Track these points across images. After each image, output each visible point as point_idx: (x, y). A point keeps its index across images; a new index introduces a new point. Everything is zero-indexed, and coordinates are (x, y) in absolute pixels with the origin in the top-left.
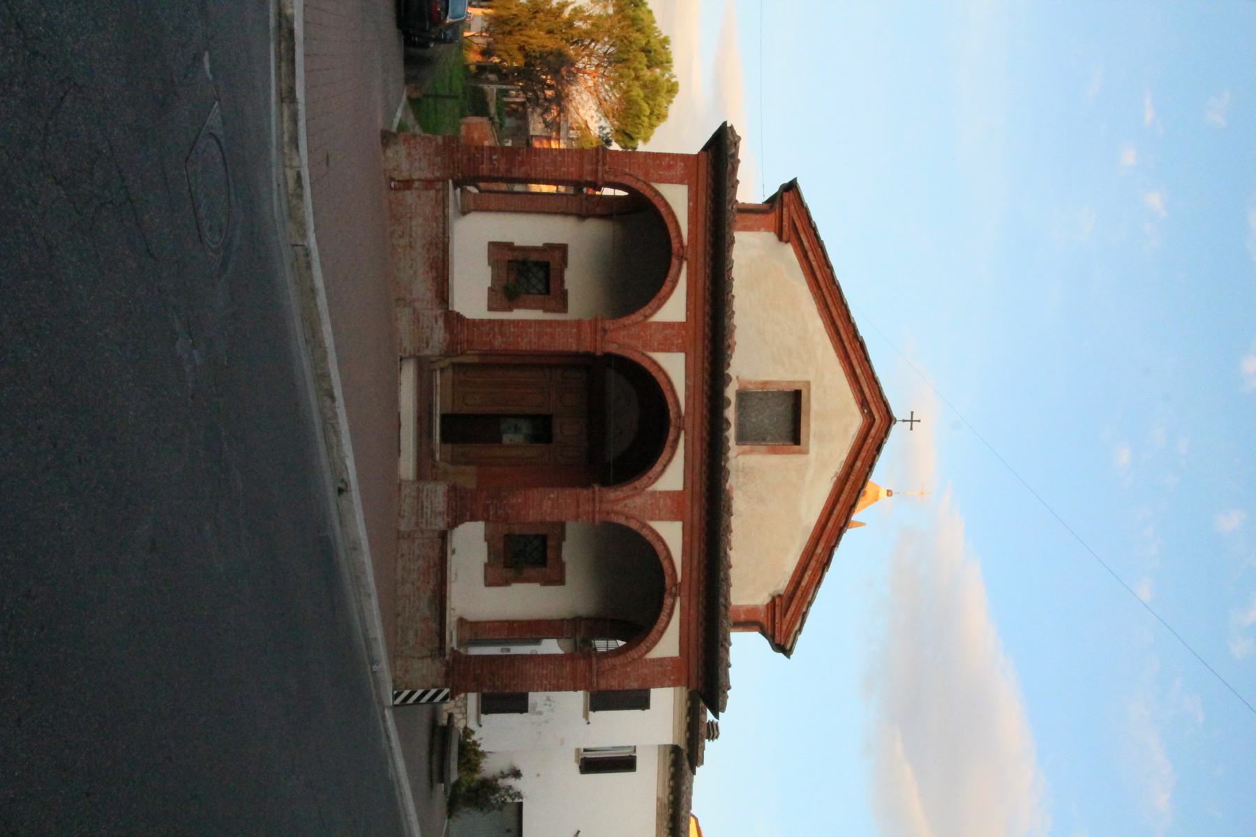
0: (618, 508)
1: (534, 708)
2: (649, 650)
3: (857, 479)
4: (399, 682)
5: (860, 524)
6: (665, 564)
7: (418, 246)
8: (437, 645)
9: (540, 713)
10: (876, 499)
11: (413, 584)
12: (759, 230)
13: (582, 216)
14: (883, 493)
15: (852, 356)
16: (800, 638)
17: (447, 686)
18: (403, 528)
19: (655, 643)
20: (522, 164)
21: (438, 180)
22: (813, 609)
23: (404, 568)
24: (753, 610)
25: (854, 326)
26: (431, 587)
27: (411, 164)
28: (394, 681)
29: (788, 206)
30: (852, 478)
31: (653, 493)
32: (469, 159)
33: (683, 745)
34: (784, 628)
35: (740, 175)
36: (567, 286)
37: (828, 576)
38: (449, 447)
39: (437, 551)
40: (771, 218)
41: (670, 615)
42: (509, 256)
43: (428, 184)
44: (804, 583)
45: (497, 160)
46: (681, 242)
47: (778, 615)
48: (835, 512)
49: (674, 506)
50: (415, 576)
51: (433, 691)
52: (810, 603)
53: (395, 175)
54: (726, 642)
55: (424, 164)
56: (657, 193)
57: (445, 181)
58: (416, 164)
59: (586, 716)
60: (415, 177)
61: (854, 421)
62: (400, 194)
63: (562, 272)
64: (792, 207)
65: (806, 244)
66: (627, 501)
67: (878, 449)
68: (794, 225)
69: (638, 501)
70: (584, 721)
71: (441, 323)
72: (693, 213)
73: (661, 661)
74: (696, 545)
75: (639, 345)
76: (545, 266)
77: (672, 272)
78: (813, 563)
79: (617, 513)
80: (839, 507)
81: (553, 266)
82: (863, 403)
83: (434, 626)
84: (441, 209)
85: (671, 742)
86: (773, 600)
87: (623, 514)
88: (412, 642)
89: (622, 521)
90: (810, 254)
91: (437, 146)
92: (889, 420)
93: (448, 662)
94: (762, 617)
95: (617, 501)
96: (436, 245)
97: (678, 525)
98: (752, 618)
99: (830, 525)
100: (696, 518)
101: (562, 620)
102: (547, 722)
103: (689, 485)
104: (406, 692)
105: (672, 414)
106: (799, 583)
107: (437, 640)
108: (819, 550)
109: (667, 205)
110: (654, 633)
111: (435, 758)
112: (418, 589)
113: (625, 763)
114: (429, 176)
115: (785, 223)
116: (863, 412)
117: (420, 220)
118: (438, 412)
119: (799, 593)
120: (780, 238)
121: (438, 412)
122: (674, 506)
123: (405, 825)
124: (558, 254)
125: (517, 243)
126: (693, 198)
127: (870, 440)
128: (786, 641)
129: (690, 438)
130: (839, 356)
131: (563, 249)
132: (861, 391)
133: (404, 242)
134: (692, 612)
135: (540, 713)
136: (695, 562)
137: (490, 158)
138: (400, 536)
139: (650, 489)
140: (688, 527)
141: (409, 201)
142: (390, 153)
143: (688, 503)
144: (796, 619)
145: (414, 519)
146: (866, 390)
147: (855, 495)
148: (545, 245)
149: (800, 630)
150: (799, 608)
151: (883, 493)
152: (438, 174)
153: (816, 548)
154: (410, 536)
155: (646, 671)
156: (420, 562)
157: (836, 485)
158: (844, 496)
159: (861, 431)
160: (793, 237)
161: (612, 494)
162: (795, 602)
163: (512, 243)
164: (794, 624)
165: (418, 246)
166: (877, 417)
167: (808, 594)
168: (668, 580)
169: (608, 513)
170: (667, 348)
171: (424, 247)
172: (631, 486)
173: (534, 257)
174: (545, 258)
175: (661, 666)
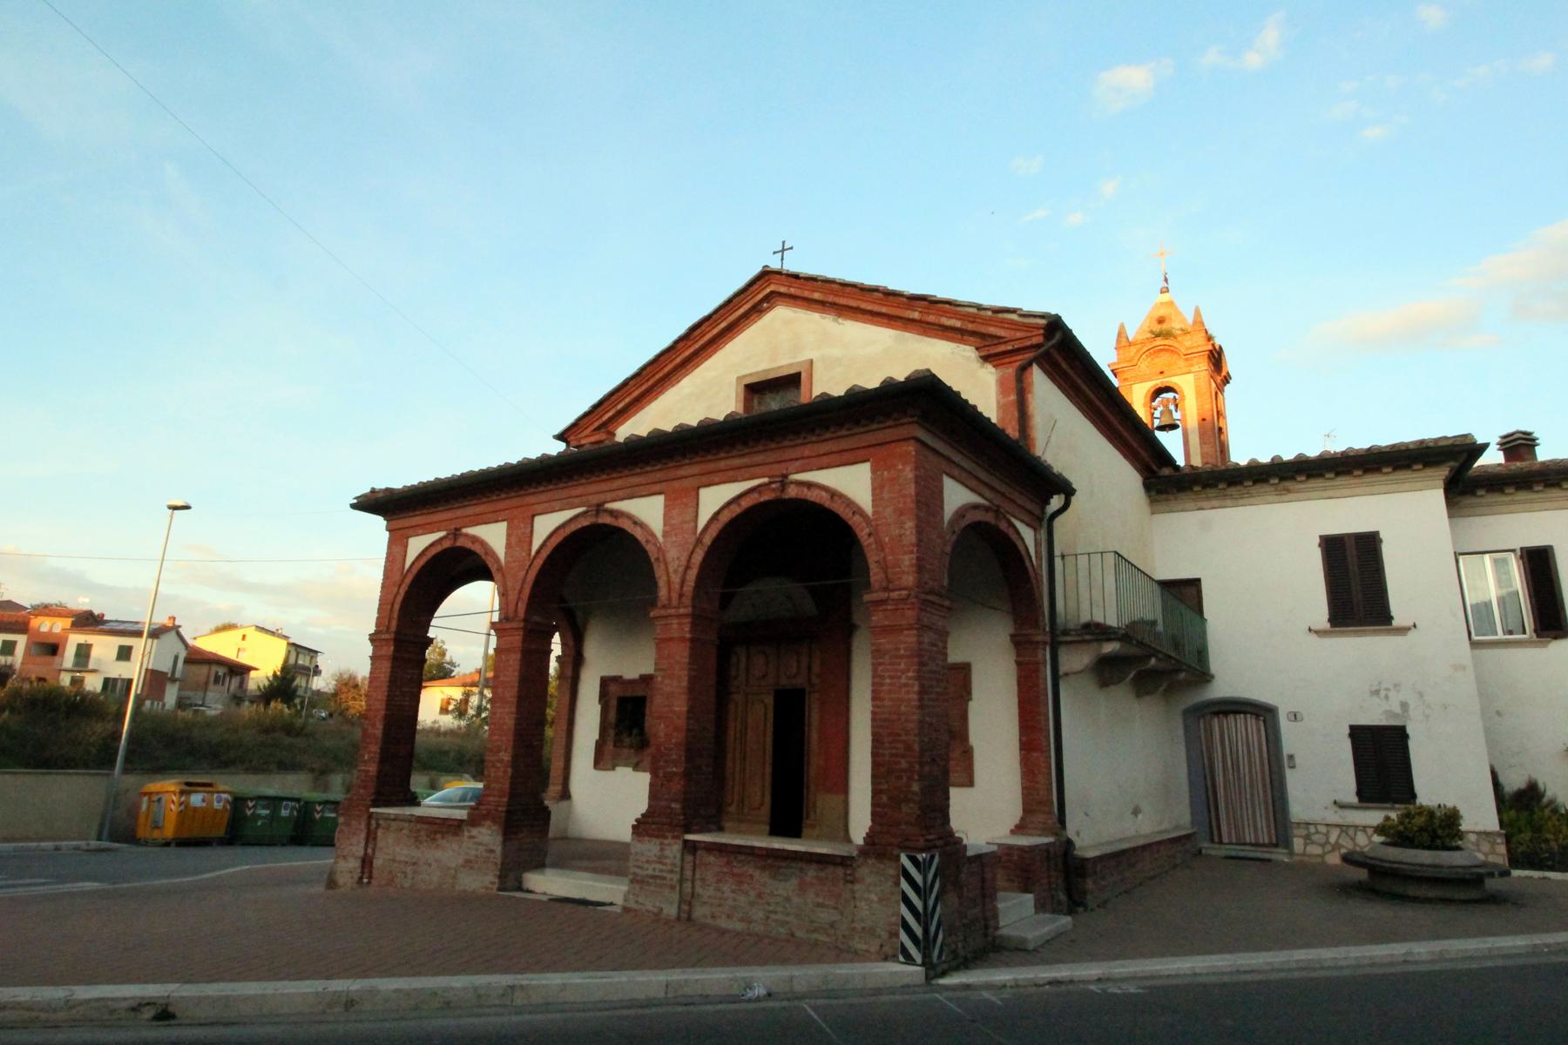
0: (676, 579)
1: (1396, 716)
3: (832, 292)
5: (1197, 312)
9: (1404, 705)
10: (1171, 303)
11: (752, 904)
14: (1165, 297)
16: (1027, 307)
17: (898, 858)
18: (671, 911)
19: (849, 503)
20: (374, 725)
21: (369, 824)
22: (986, 301)
24: (1002, 384)
26: (757, 874)
28: (886, 959)
30: (831, 299)
31: (665, 534)
33: (1443, 472)
34: (1019, 335)
35: (432, 479)
38: (805, 831)
39: (712, 859)
42: (610, 746)
43: (371, 837)
44: (958, 324)
46: (441, 539)
47: (1002, 348)
48: (869, 307)
50: (742, 898)
51: (904, 885)
52: (980, 308)
54: (1543, 463)
57: (370, 816)
59: (1403, 631)
61: (781, 315)
62: (375, 872)
70: (1412, 634)
71: (474, 831)
73: (877, 489)
74: (722, 464)
76: (622, 701)
78: (931, 318)
80: (863, 306)
82: (757, 311)
83: (812, 872)
85: (1439, 494)
88: (835, 916)
89: (692, 574)
90: (619, 407)
92: (766, 275)
94: (1010, 371)
97: (705, 494)
98: (1012, 384)
99: (884, 310)
100: (696, 469)
101: (1018, 663)
102: (1421, 695)
103: (657, 487)
104: (904, 937)
105: (585, 522)
112: (760, 895)
113: (1539, 563)
114: (363, 835)
116: (770, 309)
118: (763, 842)
119: (970, 327)
121: (763, 842)
127: (792, 291)
128: (1037, 327)
129: (609, 496)
134: (807, 453)
135: (1404, 705)
138: (685, 918)
139: (661, 539)
140: (704, 479)
143: (676, 484)
144: (1003, 321)
145: (667, 891)
149: (1013, 311)
151: (1165, 297)
152: (363, 826)
153: (913, 320)
154: (688, 901)
155: (889, 510)
156: (726, 888)
161: (663, 592)
162: (983, 329)
164: (1012, 322)
165: (416, 853)
167: (969, 315)
168: (764, 498)
169: (681, 596)
172: (655, 566)
174: (614, 703)
175: (882, 487)
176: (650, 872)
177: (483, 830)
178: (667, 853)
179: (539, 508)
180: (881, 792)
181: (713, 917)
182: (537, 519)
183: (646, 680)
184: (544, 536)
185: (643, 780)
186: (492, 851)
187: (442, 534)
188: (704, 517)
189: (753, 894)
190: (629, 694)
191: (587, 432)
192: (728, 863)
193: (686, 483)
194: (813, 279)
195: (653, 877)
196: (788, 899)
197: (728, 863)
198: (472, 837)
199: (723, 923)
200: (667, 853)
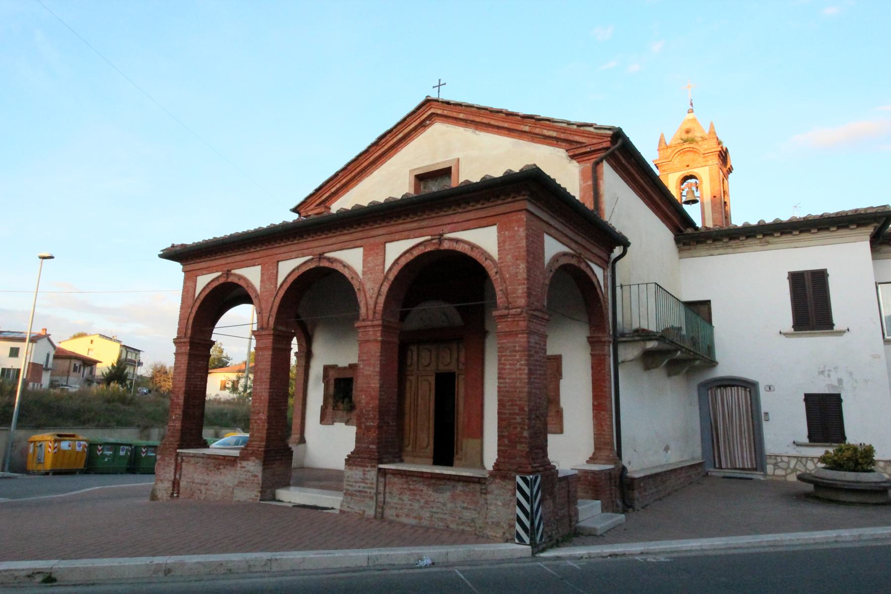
0: (371, 303)
1: (833, 387)
2: (489, 257)
3: (472, 114)
4: (508, 535)
6: (416, 253)
7: (206, 478)
9: (840, 381)
10: (695, 120)
15: (391, 143)
17: (515, 478)
18: (371, 512)
19: (483, 252)
20: (178, 397)
21: (176, 460)
23: (407, 516)
25: (370, 147)
26: (425, 488)
28: (507, 541)
30: (471, 118)
31: (364, 273)
33: (870, 230)
34: (594, 141)
36: (347, 365)
37: (543, 114)
41: (457, 241)
43: (178, 468)
44: (554, 134)
45: (176, 414)
48: (496, 124)
51: (518, 495)
52: (569, 123)
53: (170, 492)
57: (178, 454)
59: (841, 333)
60: (173, 478)
61: (438, 129)
62: (181, 491)
65: (327, 195)
66: (368, 296)
67: (509, 114)
69: (368, 286)
71: (244, 463)
72: (209, 270)
74: (400, 227)
76: (338, 381)
78: (537, 131)
79: (376, 303)
80: (493, 122)
81: (336, 376)
82: (422, 126)
83: (460, 487)
85: (867, 244)
86: (573, 157)
87: (377, 298)
90: (333, 190)
92: (428, 102)
95: (367, 304)
96: (208, 464)
97: (389, 246)
98: (590, 174)
99: (506, 125)
100: (381, 231)
101: (592, 355)
102: (851, 374)
103: (358, 243)
104: (518, 527)
106: (557, 139)
107: (472, 486)
108: (527, 129)
110: (474, 255)
111: (843, 497)
112: (426, 502)
114: (173, 467)
116: (431, 124)
119: (563, 136)
122: (375, 251)
123: (710, 553)
127: (446, 113)
130: (395, 153)
135: (840, 381)
136: (414, 225)
138: (380, 517)
142: (159, 496)
143: (372, 240)
144: (584, 132)
145: (367, 500)
146: (413, 126)
147: (483, 111)
149: (591, 125)
150: (576, 133)
151: (691, 116)
152: (173, 461)
153: (525, 132)
154: (381, 507)
157: (481, 130)
158: (485, 121)
159: (443, 122)
162: (571, 138)
164: (590, 133)
165: (206, 478)
166: (430, 112)
171: (208, 474)
173: (332, 390)
174: (332, 382)
175: (504, 242)
177: (251, 463)
182: (280, 264)
183: (352, 367)
185: (352, 430)
186: (256, 476)
187: (219, 274)
189: (422, 501)
193: (378, 240)
195: (360, 491)
197: (407, 482)
199: (404, 520)
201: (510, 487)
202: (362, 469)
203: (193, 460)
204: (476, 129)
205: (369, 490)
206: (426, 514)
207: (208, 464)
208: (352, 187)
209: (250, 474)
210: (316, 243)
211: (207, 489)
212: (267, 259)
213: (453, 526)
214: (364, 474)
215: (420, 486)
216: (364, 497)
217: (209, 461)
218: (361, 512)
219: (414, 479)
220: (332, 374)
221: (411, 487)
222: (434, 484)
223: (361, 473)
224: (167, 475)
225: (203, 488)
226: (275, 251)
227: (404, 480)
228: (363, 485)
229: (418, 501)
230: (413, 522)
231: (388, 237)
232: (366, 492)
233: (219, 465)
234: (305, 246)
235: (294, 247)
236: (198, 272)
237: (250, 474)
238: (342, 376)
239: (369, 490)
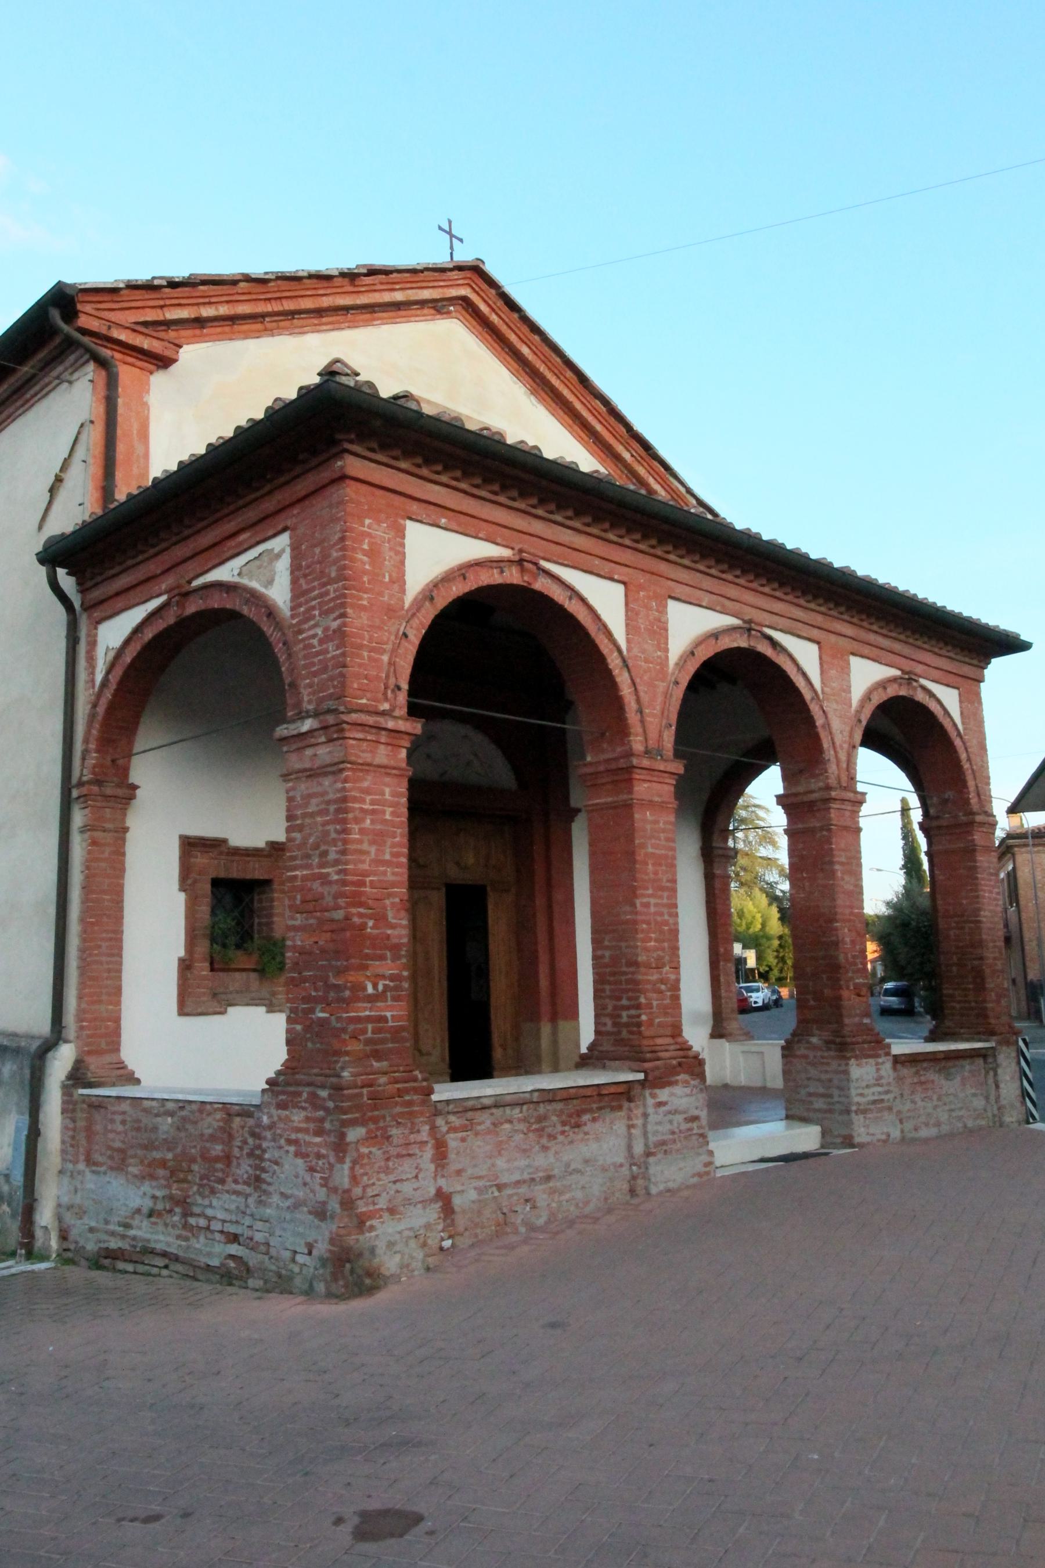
7: (541, 1161)
8: (980, 1061)
11: (935, 1107)
12: (145, 405)
13: (126, 794)
20: (380, 918)
25: (133, 287)
27: (408, 1202)
29: (112, 324)
32: (377, 1055)
38: (495, 1073)
40: (127, 373)
41: (931, 695)
42: (202, 968)
45: (375, 979)
49: (833, 660)
55: (406, 1168)
56: (428, 594)
58: (407, 1188)
61: (454, 334)
63: (237, 852)
64: (112, 316)
68: (145, 324)
71: (663, 1094)
72: (465, 524)
75: (662, 686)
77: (558, 595)
82: (438, 307)
84: (479, 1116)
91: (370, 1139)
93: (999, 1043)
96: (541, 1119)
109: (447, 578)
112: (939, 1099)
114: (429, 1152)
115: (146, 343)
117: (501, 1163)
120: (164, 362)
124: (200, 860)
125: (182, 953)
126: (436, 514)
130: (367, 323)
131: (190, 846)
132: (422, 303)
133: (540, 1193)
137: (372, 999)
141: (473, 1195)
142: (390, 1264)
148: (182, 889)
152: (424, 1133)
156: (917, 1098)
160: (172, 334)
163: (181, 961)
165: (541, 1161)
170: (660, 631)
176: (871, 1098)
177: (678, 1090)
178: (883, 1073)
179: (679, 590)
180: (665, 1010)
181: (916, 1129)
182: (621, 588)
183: (275, 848)
184: (939, 695)
185: (278, 1023)
186: (695, 1118)
187: (505, 553)
188: (857, 692)
189: (935, 1097)
190: (235, 874)
191: (131, 317)
192: (917, 1073)
193: (842, 642)
194: (535, 329)
195: (874, 1102)
196: (955, 1096)
197: (917, 1073)
198: (661, 1104)
199: (924, 1133)
200: (883, 1073)
201: (1014, 1054)
202: (871, 1061)
203: (485, 1120)
204: (533, 392)
205: (885, 1097)
206: (944, 1117)
207: (541, 1119)
208: (246, 336)
209: (679, 1118)
210: (749, 597)
211: (553, 1191)
212: (642, 579)
213: (970, 1124)
214: (878, 1070)
215: (932, 1076)
216: (880, 1110)
217: (542, 1109)
218: (884, 1137)
219: (925, 1065)
220: (211, 866)
221: (923, 1079)
222: (944, 1067)
223: (874, 1069)
224: (407, 1188)
225: (540, 1193)
226: (663, 567)
227: (914, 1070)
228: (880, 1089)
229: (931, 1099)
230: (933, 1132)
231: (855, 646)
232: (882, 1101)
233: (579, 1113)
234: (733, 591)
235: (707, 583)
236: (415, 507)
237: (679, 1118)
238: (236, 872)
239: (885, 1097)
